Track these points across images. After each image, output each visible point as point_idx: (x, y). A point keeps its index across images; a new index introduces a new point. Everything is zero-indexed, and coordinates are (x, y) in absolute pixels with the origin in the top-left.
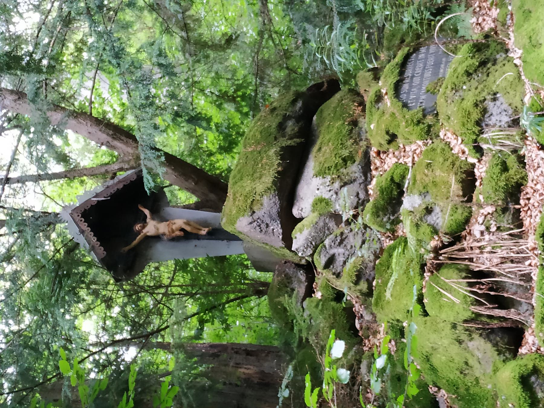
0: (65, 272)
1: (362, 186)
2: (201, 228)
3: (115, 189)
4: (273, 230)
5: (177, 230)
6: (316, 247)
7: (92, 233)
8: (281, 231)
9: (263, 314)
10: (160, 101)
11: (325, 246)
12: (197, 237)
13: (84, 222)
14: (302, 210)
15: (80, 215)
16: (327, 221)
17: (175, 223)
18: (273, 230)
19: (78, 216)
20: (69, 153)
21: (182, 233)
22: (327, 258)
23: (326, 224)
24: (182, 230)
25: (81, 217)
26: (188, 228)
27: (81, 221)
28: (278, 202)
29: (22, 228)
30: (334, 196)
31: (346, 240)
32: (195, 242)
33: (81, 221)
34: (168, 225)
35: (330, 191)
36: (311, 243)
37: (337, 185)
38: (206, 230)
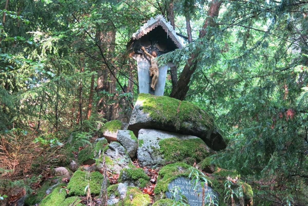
1: (149, 163)
2: (154, 84)
3: (174, 40)
4: (134, 120)
6: (120, 142)
7: (149, 32)
8: (133, 124)
11: (119, 146)
12: (150, 83)
14: (141, 133)
16: (132, 146)
18: (134, 120)
21: (151, 75)
22: (113, 147)
23: (130, 146)
24: (153, 75)
26: (153, 78)
28: (146, 121)
30: (145, 149)
31: (122, 157)
32: (148, 82)
35: (148, 147)
36: (121, 139)
37: (150, 150)
38: (153, 87)
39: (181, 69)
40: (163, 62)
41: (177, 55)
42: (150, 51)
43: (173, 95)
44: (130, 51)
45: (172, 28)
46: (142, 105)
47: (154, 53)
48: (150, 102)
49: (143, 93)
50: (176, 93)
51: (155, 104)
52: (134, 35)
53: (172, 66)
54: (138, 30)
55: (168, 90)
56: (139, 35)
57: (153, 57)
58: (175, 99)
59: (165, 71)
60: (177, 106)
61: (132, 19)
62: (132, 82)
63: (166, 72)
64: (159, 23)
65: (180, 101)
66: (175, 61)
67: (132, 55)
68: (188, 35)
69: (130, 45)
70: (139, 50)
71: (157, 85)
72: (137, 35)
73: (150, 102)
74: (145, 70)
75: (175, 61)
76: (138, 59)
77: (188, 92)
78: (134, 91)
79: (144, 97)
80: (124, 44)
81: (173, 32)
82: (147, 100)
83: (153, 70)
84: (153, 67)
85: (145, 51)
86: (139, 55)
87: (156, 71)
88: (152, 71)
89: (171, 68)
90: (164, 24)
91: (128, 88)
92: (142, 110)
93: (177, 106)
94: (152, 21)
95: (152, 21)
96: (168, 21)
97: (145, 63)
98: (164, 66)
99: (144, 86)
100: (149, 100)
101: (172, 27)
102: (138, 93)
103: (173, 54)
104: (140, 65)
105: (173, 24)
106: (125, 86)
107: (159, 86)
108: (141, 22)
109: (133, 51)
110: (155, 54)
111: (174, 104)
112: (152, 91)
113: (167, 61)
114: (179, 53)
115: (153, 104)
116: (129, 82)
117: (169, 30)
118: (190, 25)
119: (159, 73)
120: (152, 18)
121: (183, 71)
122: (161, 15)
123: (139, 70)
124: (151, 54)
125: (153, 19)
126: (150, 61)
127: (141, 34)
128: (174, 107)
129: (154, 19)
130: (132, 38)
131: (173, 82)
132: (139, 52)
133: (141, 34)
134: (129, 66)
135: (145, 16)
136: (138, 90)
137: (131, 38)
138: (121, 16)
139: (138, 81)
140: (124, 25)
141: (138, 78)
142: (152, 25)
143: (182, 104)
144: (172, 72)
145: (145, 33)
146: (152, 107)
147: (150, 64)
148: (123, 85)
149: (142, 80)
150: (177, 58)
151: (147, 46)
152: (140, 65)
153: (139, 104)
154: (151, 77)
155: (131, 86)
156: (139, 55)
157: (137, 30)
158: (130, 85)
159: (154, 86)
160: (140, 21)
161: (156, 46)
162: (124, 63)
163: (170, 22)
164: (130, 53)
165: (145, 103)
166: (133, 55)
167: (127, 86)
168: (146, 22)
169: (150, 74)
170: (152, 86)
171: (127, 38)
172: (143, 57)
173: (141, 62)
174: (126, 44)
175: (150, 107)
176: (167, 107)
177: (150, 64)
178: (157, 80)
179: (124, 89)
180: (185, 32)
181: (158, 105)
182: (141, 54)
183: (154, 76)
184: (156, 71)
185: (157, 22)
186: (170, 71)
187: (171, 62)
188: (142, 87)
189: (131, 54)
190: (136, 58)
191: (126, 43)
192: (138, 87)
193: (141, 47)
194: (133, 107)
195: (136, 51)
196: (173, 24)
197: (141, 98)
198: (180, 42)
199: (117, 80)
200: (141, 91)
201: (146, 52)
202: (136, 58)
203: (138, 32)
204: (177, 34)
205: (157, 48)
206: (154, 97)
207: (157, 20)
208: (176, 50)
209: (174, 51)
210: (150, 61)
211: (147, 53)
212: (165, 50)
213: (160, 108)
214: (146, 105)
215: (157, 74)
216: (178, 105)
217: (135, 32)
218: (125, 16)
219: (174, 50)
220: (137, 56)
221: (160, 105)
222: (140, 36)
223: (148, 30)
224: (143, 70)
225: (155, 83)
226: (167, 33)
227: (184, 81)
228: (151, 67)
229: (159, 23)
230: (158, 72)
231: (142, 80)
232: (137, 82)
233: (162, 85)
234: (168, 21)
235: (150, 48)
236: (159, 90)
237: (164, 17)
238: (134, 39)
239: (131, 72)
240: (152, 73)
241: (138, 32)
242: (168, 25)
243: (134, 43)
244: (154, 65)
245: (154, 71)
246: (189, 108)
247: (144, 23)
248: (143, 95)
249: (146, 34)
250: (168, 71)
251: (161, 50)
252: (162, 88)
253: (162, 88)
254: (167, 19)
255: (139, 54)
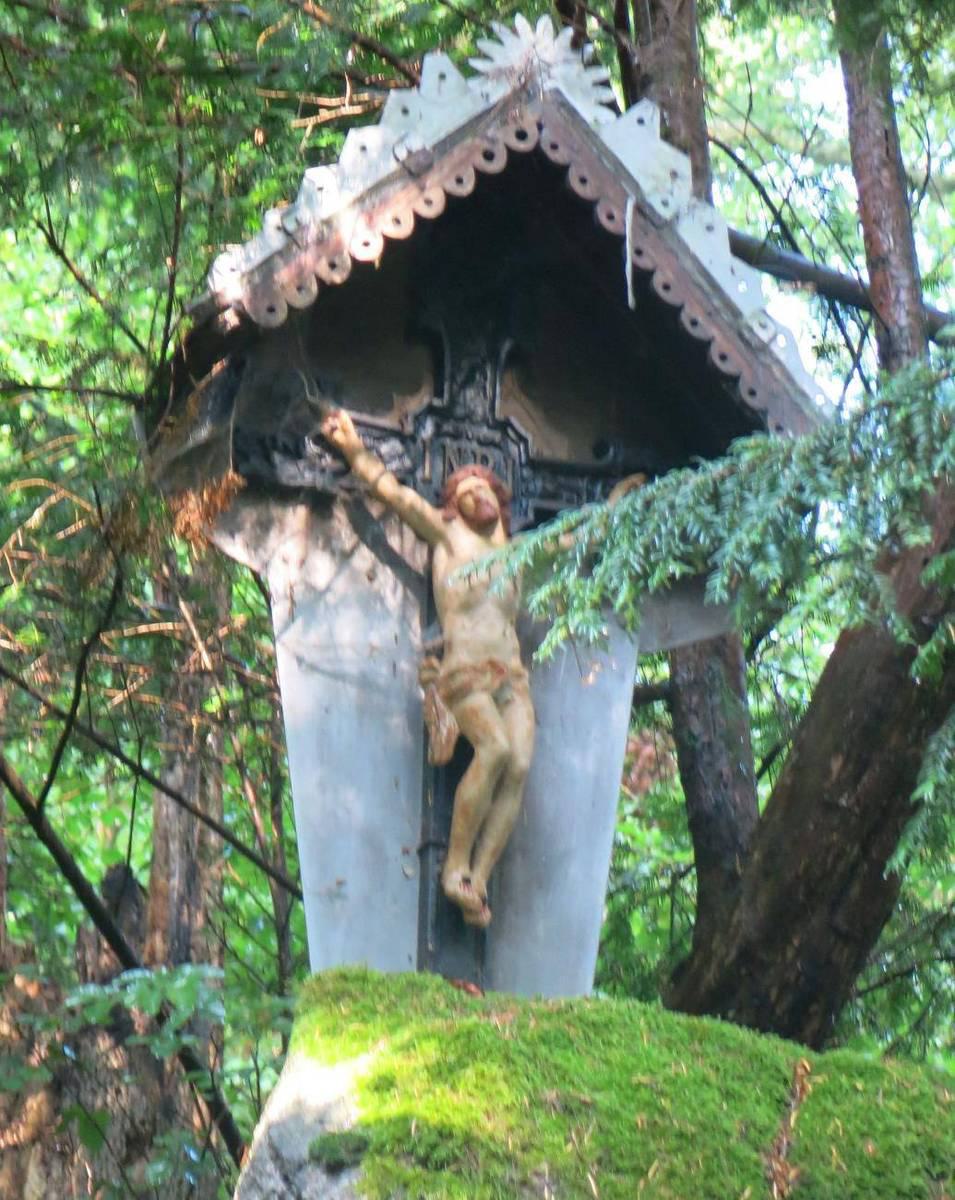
0: (77, 129)
2: (485, 860)
5: (463, 719)
7: (405, 230)
9: (39, 755)
10: (890, 1082)
12: (433, 847)
13: (480, 175)
15: (523, 146)
17: (646, 234)
19: (522, 135)
20: (524, 1149)
21: (442, 751)
24: (464, 750)
25: (511, 152)
26: (473, 786)
27: (489, 156)
29: (158, 943)
32: (403, 830)
33: (489, 156)
34: (495, 667)
39: (801, 653)
40: (590, 592)
41: (764, 506)
42: (427, 464)
43: (710, 976)
44: (188, 469)
45: (686, 185)
46: (354, 1111)
47: (473, 484)
48: (443, 1073)
49: (354, 966)
50: (746, 955)
51: (508, 1096)
52: (230, 278)
53: (693, 632)
54: (273, 217)
55: (637, 924)
56: (283, 275)
57: (462, 537)
58: (743, 1035)
59: (606, 702)
60: (763, 1114)
61: (197, 71)
62: (198, 832)
63: (623, 708)
64: (529, 119)
65: (804, 1056)
66: (741, 580)
67: (209, 513)
68: (876, 262)
69: (184, 389)
70: (296, 453)
71: (519, 872)
72: (266, 267)
73: (443, 1073)
74: (365, 683)
75: (741, 580)
76: (284, 556)
77: (889, 934)
78: (236, 940)
79: (366, 1015)
80: (101, 374)
81: (690, 232)
82: (407, 1048)
83: (464, 691)
84: (460, 657)
85: (366, 466)
86: (296, 516)
87: (500, 701)
88: (454, 697)
89: (673, 657)
90: (589, 134)
91: (151, 906)
92: (346, 1180)
93: (763, 1114)
94: (438, 104)
95: (438, 104)
96: (632, 99)
97: (370, 602)
98: (603, 641)
99: (357, 885)
100: (430, 1050)
101: (684, 164)
102: (289, 964)
103: (715, 498)
104: (315, 635)
105: (687, 133)
106: (121, 878)
107: (544, 878)
108: (310, 110)
109: (217, 470)
110: (489, 496)
111: (728, 1095)
112: (458, 941)
113: (640, 579)
114: (786, 482)
115: (479, 1105)
116: (161, 836)
117: (642, 210)
118: (891, 138)
119: (539, 719)
120: (435, 63)
121: (821, 690)
122: (545, 23)
123: (297, 693)
124: (441, 498)
125: (454, 75)
126: (423, 588)
127: (307, 258)
128: (732, 1125)
129: (468, 72)
130: (208, 313)
131: (705, 825)
132: (294, 473)
133: (307, 258)
134: (161, 638)
135: (349, 39)
136: (281, 925)
137: (195, 312)
138: (53, 35)
139: (277, 818)
140: (90, 149)
141: (278, 781)
142: (445, 146)
143: (823, 1091)
144: (690, 706)
145: (364, 241)
146: (469, 1141)
147: (431, 614)
148: (93, 868)
149: (339, 806)
150: (758, 552)
151: (381, 405)
152: (315, 635)
153: (315, 1101)
154: (443, 774)
155: (192, 876)
156: (296, 516)
157: (261, 208)
158: (177, 866)
159: (479, 879)
160: (289, 103)
161: (494, 397)
162: (114, 611)
163: (647, 109)
164: (179, 493)
165: (384, 1085)
166: (221, 517)
167: (144, 879)
168: (371, 115)
169: (424, 733)
170: (453, 884)
171: (142, 313)
172: (346, 536)
173: (317, 595)
174: (137, 379)
175: (444, 1134)
176: (654, 1130)
177: (431, 614)
178: (509, 808)
179: (115, 906)
180: (823, 199)
181: (537, 1103)
182: (320, 504)
183: (484, 757)
184: (500, 701)
185: (500, 112)
186: (668, 693)
187: (690, 587)
188: (335, 892)
189: (193, 501)
190: (257, 543)
191: (125, 363)
192: (288, 889)
193: (318, 415)
194: (236, 1144)
195: (256, 462)
196: (687, 133)
197: (333, 1031)
198: (779, 347)
199: (35, 814)
200: (327, 947)
201: (378, 472)
202: (257, 543)
203: (276, 241)
204: (744, 249)
205: (504, 426)
206: (490, 1017)
207: (499, 91)
208: (747, 449)
209: (716, 468)
210: (423, 588)
211: (388, 485)
212: (600, 450)
213: (562, 1146)
214: (393, 1107)
215: (507, 733)
216: (782, 1106)
217: (231, 230)
218: (111, 38)
219: (716, 452)
220: (264, 526)
221: (569, 1110)
222: (294, 291)
223: (398, 218)
224: (351, 692)
225: (491, 843)
226: (620, 240)
227: (831, 807)
228: (440, 653)
229: (529, 119)
230: (521, 713)
231: (339, 806)
232: (269, 834)
233: (574, 870)
234: (632, 99)
235: (428, 430)
236: (541, 928)
237: (577, 43)
238: (231, 319)
239: (194, 706)
240: (447, 726)
241: (276, 241)
242: (635, 141)
243: (236, 367)
244: (479, 634)
245: (480, 700)
246: (905, 1140)
247: (343, 125)
248: (352, 993)
249: (372, 253)
250: (643, 697)
251: (558, 448)
252: (582, 896)
253: (582, 896)
254: (610, 71)
255: (288, 495)
